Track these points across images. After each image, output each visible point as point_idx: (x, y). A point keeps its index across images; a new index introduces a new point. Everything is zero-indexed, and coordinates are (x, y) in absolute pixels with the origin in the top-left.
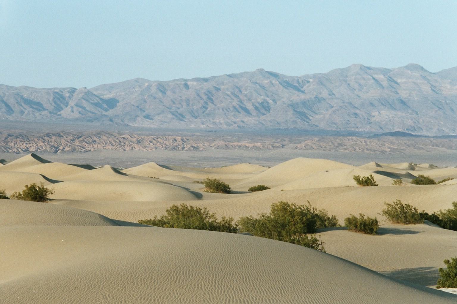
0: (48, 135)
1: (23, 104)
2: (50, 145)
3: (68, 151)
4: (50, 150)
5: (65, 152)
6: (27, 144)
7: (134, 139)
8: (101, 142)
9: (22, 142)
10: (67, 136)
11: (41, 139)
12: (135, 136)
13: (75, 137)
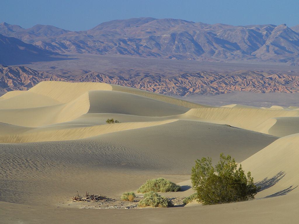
1: (214, 44)
4: (176, 92)
7: (282, 80)
8: (243, 83)
10: (207, 76)
11: (173, 80)
12: (285, 76)
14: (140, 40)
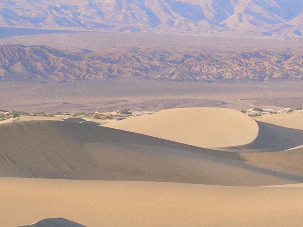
0: (244, 55)
2: (250, 69)
3: (278, 78)
4: (253, 77)
5: (274, 79)
6: (217, 68)
9: (211, 66)
11: (236, 61)
13: (280, 58)
14: (76, 7)
